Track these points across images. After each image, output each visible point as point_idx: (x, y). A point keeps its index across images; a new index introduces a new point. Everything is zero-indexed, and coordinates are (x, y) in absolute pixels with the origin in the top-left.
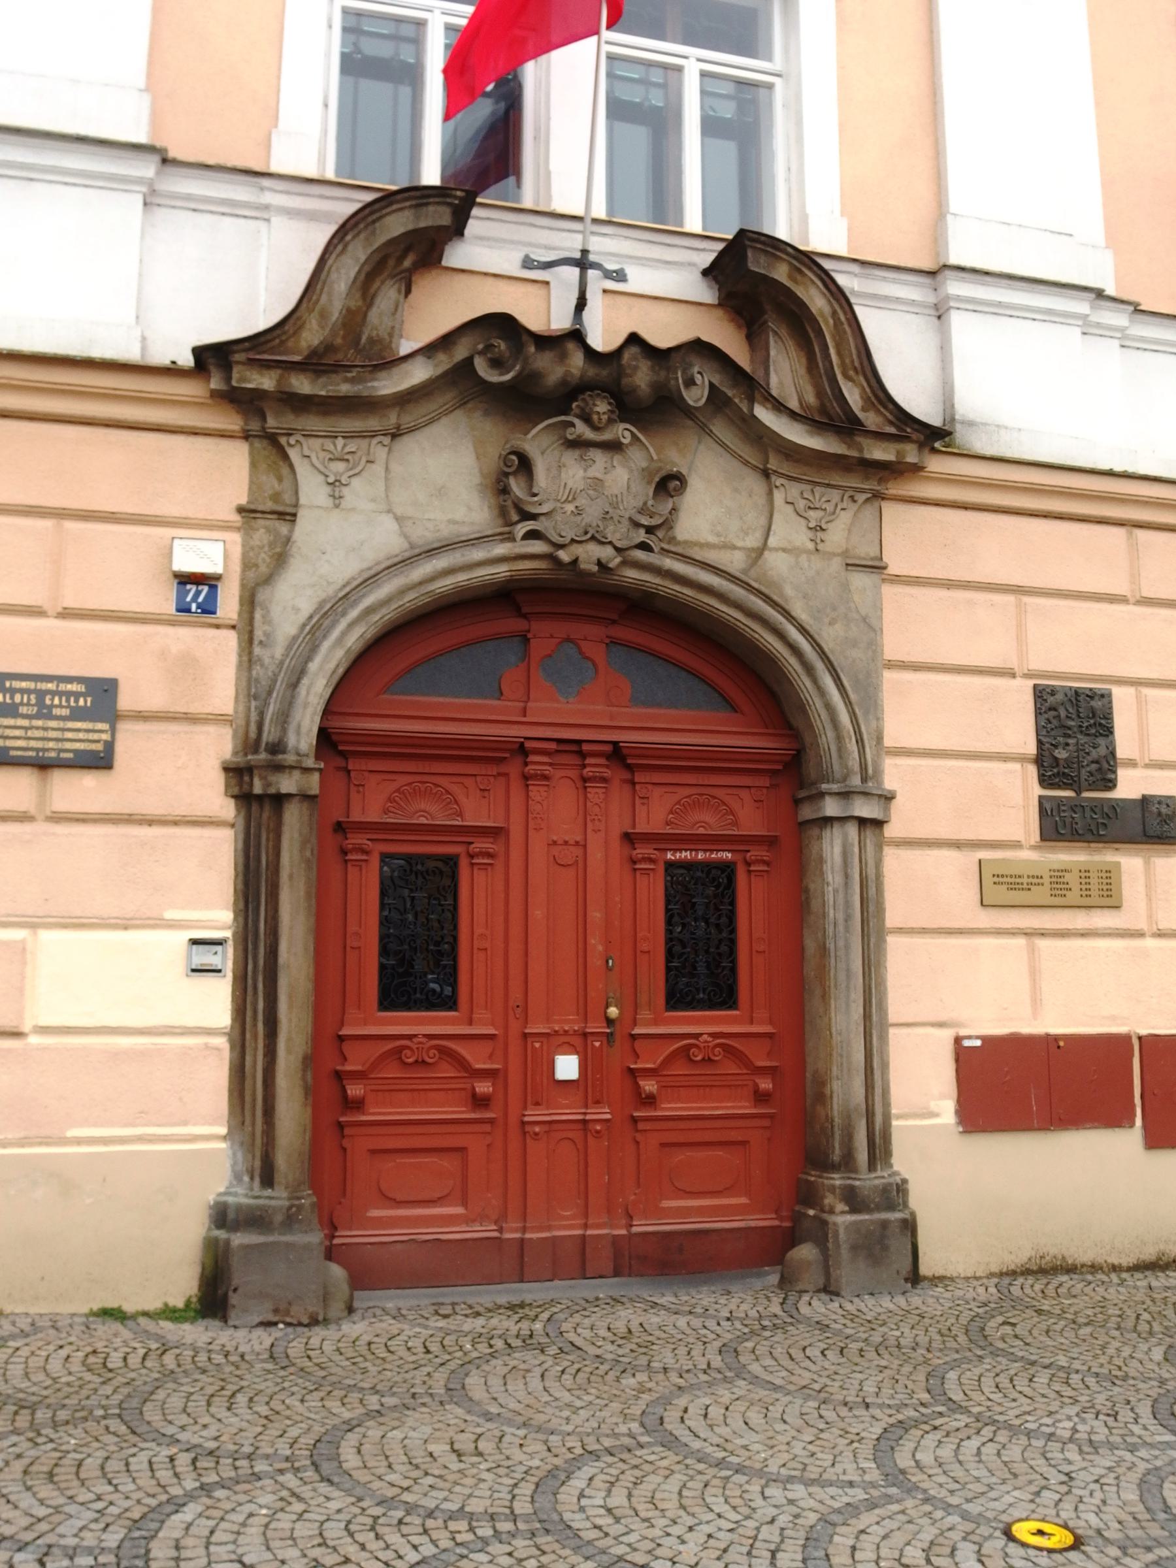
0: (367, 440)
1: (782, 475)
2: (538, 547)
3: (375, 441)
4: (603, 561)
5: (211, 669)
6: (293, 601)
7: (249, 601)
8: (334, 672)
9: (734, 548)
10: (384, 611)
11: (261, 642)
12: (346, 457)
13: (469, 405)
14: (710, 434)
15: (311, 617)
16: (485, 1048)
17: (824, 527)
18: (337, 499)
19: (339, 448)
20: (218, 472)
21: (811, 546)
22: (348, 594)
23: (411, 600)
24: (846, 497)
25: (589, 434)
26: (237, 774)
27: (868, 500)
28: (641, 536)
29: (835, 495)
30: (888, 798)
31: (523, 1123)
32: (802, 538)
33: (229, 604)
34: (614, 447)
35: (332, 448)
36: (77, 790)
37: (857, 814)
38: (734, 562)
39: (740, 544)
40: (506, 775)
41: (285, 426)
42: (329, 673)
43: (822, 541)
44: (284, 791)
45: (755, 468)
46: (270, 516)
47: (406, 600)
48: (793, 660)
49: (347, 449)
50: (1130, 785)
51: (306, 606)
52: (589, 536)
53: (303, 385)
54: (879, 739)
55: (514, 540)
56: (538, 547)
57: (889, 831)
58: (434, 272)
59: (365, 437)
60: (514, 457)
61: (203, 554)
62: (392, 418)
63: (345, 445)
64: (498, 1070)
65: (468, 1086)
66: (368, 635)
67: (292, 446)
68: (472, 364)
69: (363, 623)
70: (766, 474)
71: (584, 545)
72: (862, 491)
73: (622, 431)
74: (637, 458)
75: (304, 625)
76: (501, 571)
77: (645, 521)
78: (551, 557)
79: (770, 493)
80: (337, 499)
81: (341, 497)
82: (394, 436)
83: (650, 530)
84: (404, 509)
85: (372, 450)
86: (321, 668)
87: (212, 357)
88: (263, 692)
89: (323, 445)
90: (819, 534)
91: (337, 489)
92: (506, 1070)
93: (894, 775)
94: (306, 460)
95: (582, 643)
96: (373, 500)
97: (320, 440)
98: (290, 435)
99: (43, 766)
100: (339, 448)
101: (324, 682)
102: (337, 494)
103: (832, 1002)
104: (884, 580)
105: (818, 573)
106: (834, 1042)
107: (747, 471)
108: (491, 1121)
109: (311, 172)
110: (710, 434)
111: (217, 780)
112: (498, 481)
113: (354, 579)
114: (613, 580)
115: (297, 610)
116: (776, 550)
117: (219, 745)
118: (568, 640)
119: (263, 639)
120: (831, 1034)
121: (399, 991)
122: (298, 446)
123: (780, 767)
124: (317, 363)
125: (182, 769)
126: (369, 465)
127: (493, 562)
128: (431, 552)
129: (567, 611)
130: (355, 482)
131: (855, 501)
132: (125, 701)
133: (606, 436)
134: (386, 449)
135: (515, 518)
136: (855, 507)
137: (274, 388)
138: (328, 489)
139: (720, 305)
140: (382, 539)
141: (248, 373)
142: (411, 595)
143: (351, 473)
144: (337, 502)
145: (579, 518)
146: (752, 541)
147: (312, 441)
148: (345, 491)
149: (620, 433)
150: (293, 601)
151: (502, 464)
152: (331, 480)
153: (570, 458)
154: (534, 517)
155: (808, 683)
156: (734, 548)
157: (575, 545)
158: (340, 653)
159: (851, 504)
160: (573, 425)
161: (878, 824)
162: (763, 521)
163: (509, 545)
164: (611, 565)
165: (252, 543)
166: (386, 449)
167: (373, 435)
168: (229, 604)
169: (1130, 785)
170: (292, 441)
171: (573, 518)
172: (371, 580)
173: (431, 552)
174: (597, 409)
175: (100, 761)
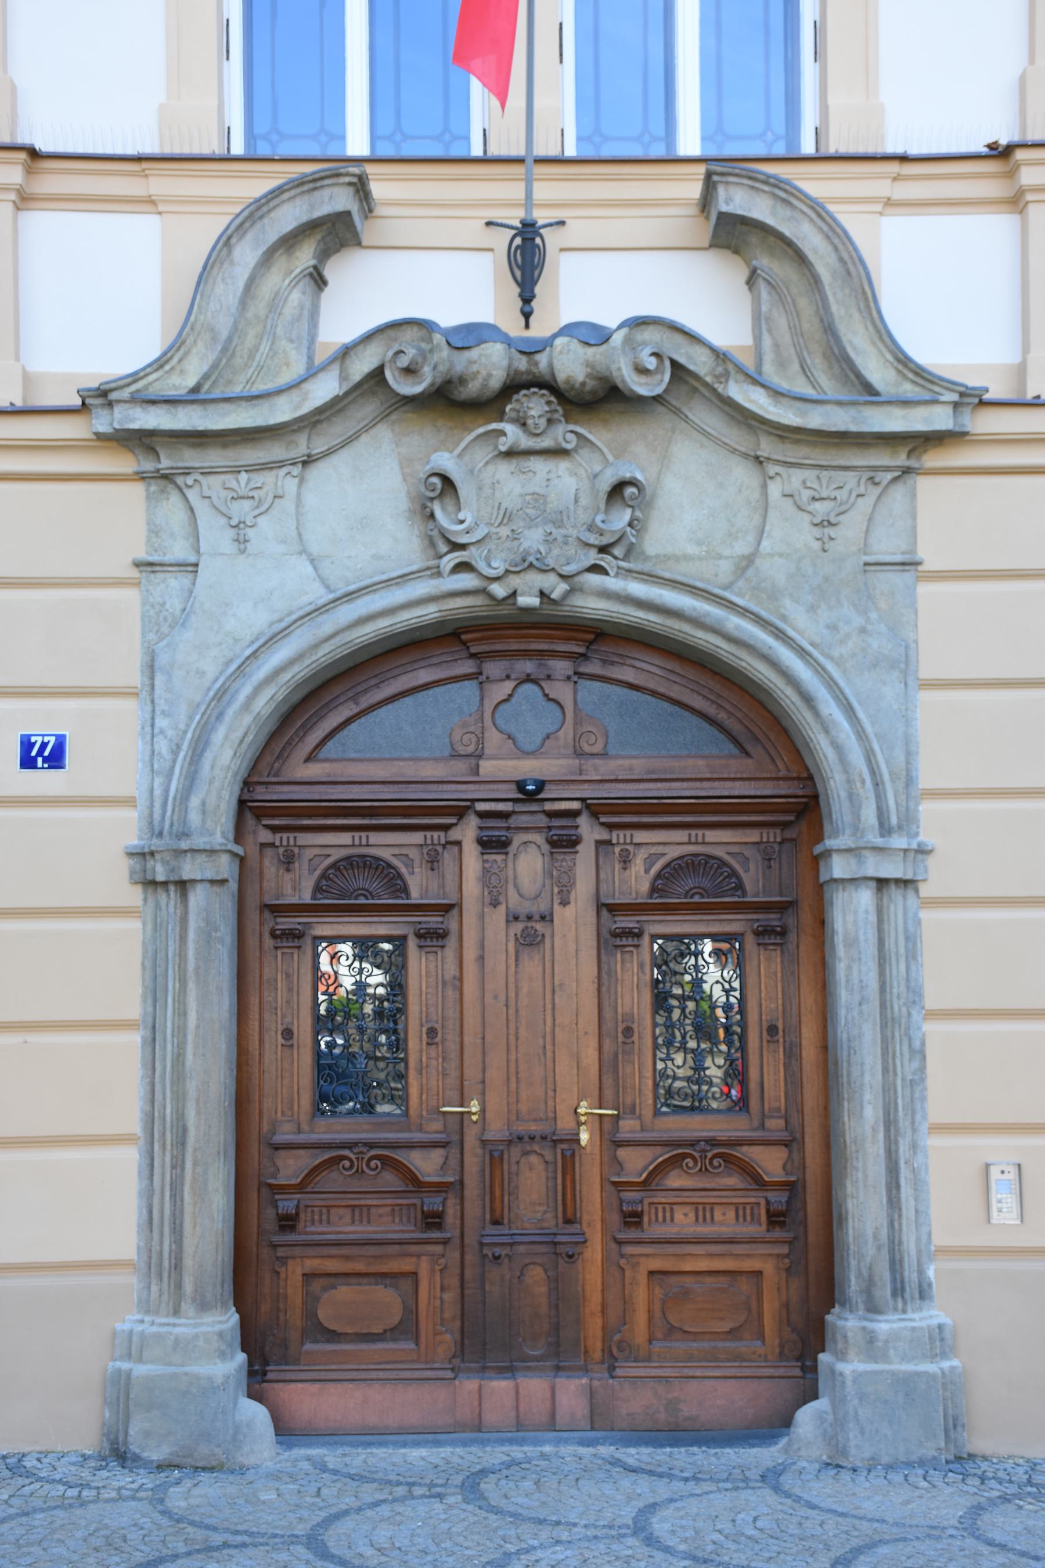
0: (274, 472)
1: (778, 462)
2: (466, 581)
3: (282, 472)
4: (547, 592)
8: (242, 741)
9: (720, 557)
10: (296, 668)
11: (163, 712)
12: (251, 494)
13: (394, 417)
14: (686, 419)
15: (216, 680)
16: (437, 1156)
17: (833, 520)
18: (241, 542)
19: (243, 483)
21: (817, 545)
22: (256, 651)
23: (325, 654)
24: (863, 481)
25: (526, 442)
27: (895, 480)
28: (593, 557)
29: (850, 479)
30: (923, 851)
31: (482, 1245)
32: (805, 536)
34: (558, 452)
35: (233, 484)
37: (871, 872)
38: (716, 573)
39: (726, 552)
40: (459, 843)
41: (180, 465)
42: (237, 742)
43: (832, 539)
44: (185, 878)
45: (745, 455)
47: (320, 654)
48: (789, 691)
49: (252, 485)
51: (210, 667)
52: (526, 564)
54: (910, 781)
55: (439, 574)
56: (466, 581)
57: (925, 890)
59: (271, 468)
60: (435, 480)
62: (301, 446)
63: (249, 480)
64: (451, 1183)
65: (417, 1201)
66: (280, 697)
67: (190, 487)
68: (383, 372)
69: (273, 685)
70: (758, 460)
71: (522, 574)
72: (887, 469)
73: (561, 434)
74: (587, 461)
75: (209, 689)
76: (430, 612)
77: (593, 539)
78: (483, 591)
79: (764, 486)
80: (241, 542)
81: (246, 541)
82: (305, 463)
83: (603, 549)
85: (280, 483)
86: (226, 738)
89: (224, 483)
90: (827, 530)
91: (242, 532)
92: (461, 1182)
93: (934, 822)
94: (206, 501)
95: (543, 683)
96: (283, 542)
97: (222, 477)
98: (189, 473)
100: (243, 483)
101: (231, 753)
102: (241, 538)
103: (846, 1104)
104: (918, 579)
105: (826, 579)
106: (848, 1152)
107: (736, 459)
108: (445, 1242)
109: (212, 146)
110: (686, 419)
111: (123, 866)
112: (424, 507)
113: (262, 633)
114: (564, 610)
115: (201, 673)
116: (771, 555)
118: (528, 679)
119: (166, 708)
120: (845, 1141)
122: (198, 485)
123: (792, 818)
126: (277, 500)
127: (422, 598)
128: (349, 596)
130: (262, 521)
131: (876, 484)
133: (546, 443)
134: (297, 480)
135: (443, 548)
136: (876, 491)
138: (232, 533)
139: (712, 246)
141: (131, 412)
142: (327, 648)
143: (256, 512)
144: (242, 546)
145: (516, 543)
146: (742, 548)
147: (212, 479)
148: (251, 533)
149: (561, 440)
151: (423, 489)
152: (234, 523)
153: (504, 470)
154: (463, 547)
155: (808, 716)
156: (720, 557)
157: (511, 576)
158: (247, 719)
159: (871, 488)
160: (502, 433)
161: (905, 883)
162: (757, 519)
163: (434, 582)
164: (553, 596)
165: (151, 600)
166: (297, 480)
167: (280, 464)
170: (190, 481)
171: (508, 544)
173: (349, 596)
174: (532, 413)
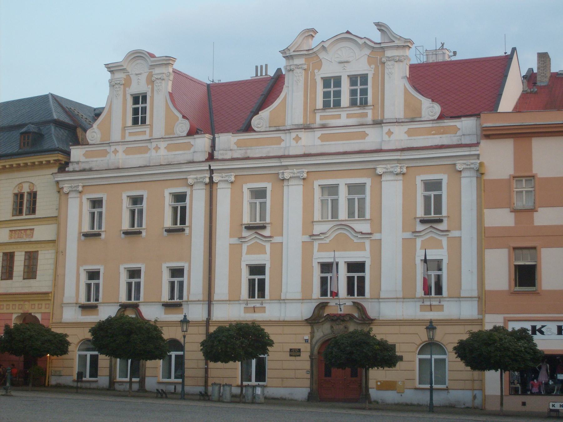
5: (308, 346)
6: (314, 341)
7: (311, 341)
20: (308, 329)
26: (310, 356)
33: (309, 341)
36: (298, 358)
46: (312, 334)
50: (486, 211)
53: (313, 322)
58: (135, 94)
61: (307, 337)
73: (341, 323)
84: (324, 331)
87: (306, 320)
88: (312, 349)
99: (295, 356)
117: (309, 354)
121: (326, 375)
124: (314, 320)
125: (305, 355)
129: (116, 182)
132: (301, 350)
137: (313, 321)
140: (322, 334)
150: (314, 341)
168: (309, 341)
169: (486, 211)
172: (320, 339)
175: (300, 356)
